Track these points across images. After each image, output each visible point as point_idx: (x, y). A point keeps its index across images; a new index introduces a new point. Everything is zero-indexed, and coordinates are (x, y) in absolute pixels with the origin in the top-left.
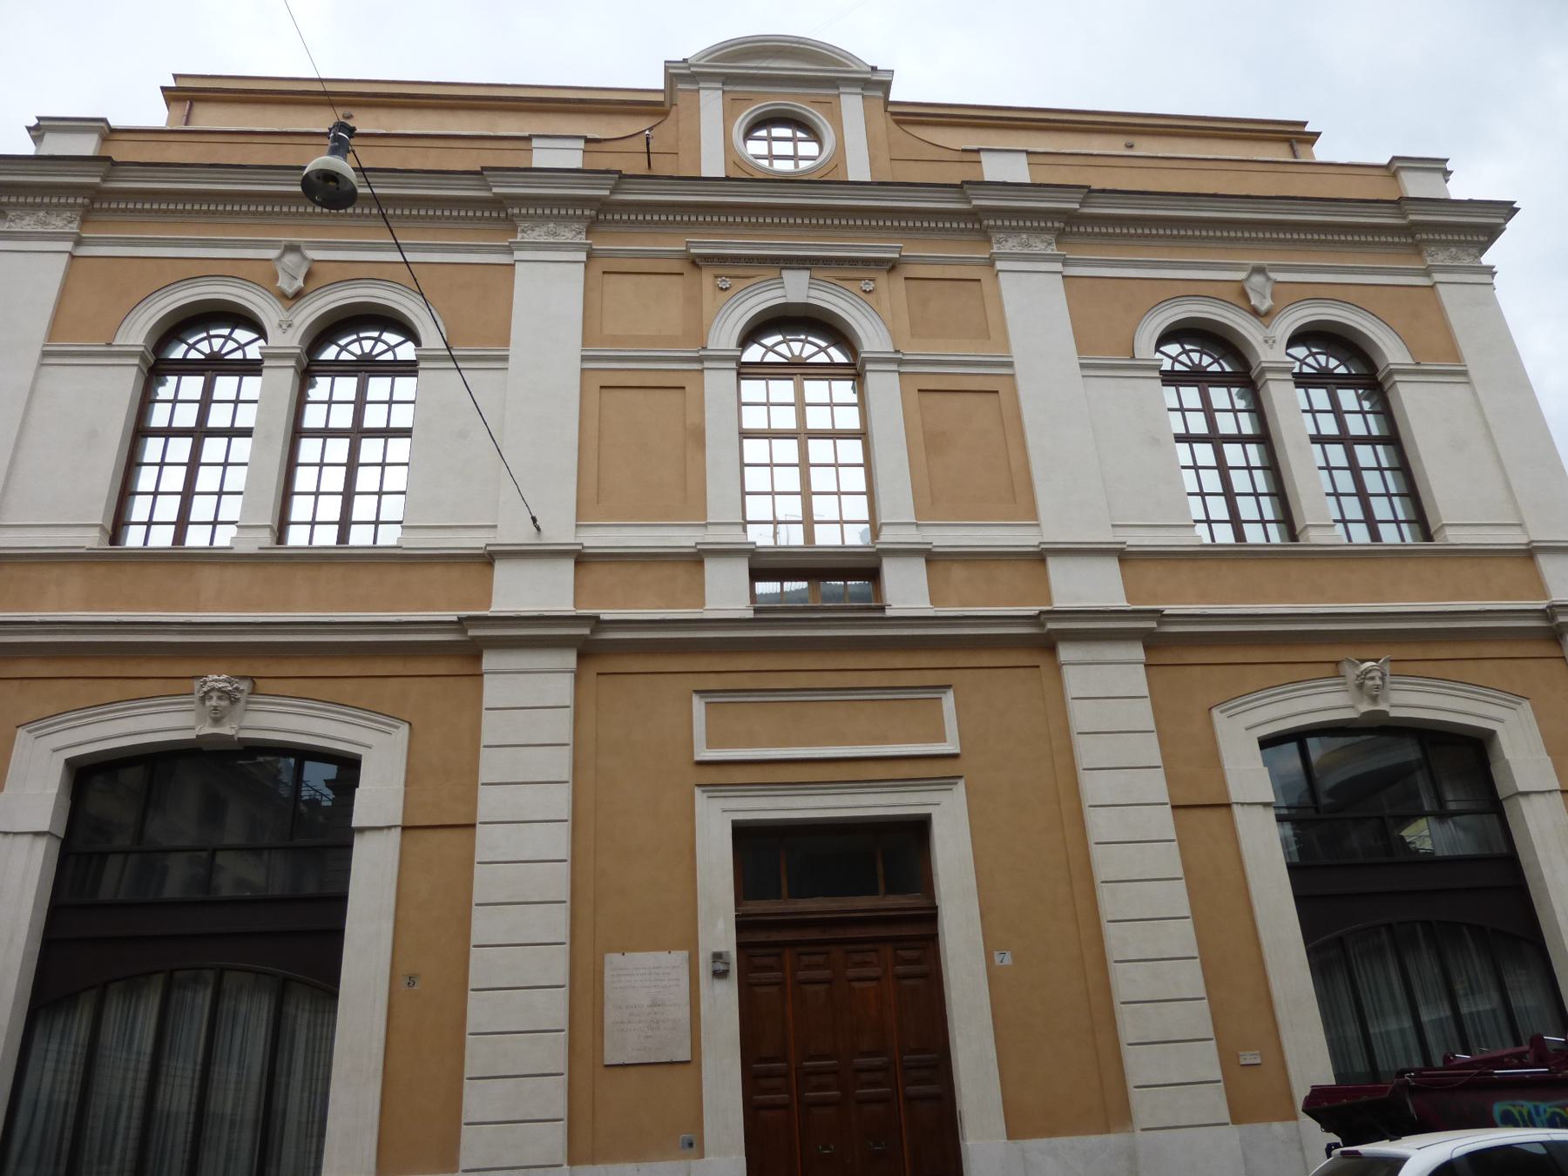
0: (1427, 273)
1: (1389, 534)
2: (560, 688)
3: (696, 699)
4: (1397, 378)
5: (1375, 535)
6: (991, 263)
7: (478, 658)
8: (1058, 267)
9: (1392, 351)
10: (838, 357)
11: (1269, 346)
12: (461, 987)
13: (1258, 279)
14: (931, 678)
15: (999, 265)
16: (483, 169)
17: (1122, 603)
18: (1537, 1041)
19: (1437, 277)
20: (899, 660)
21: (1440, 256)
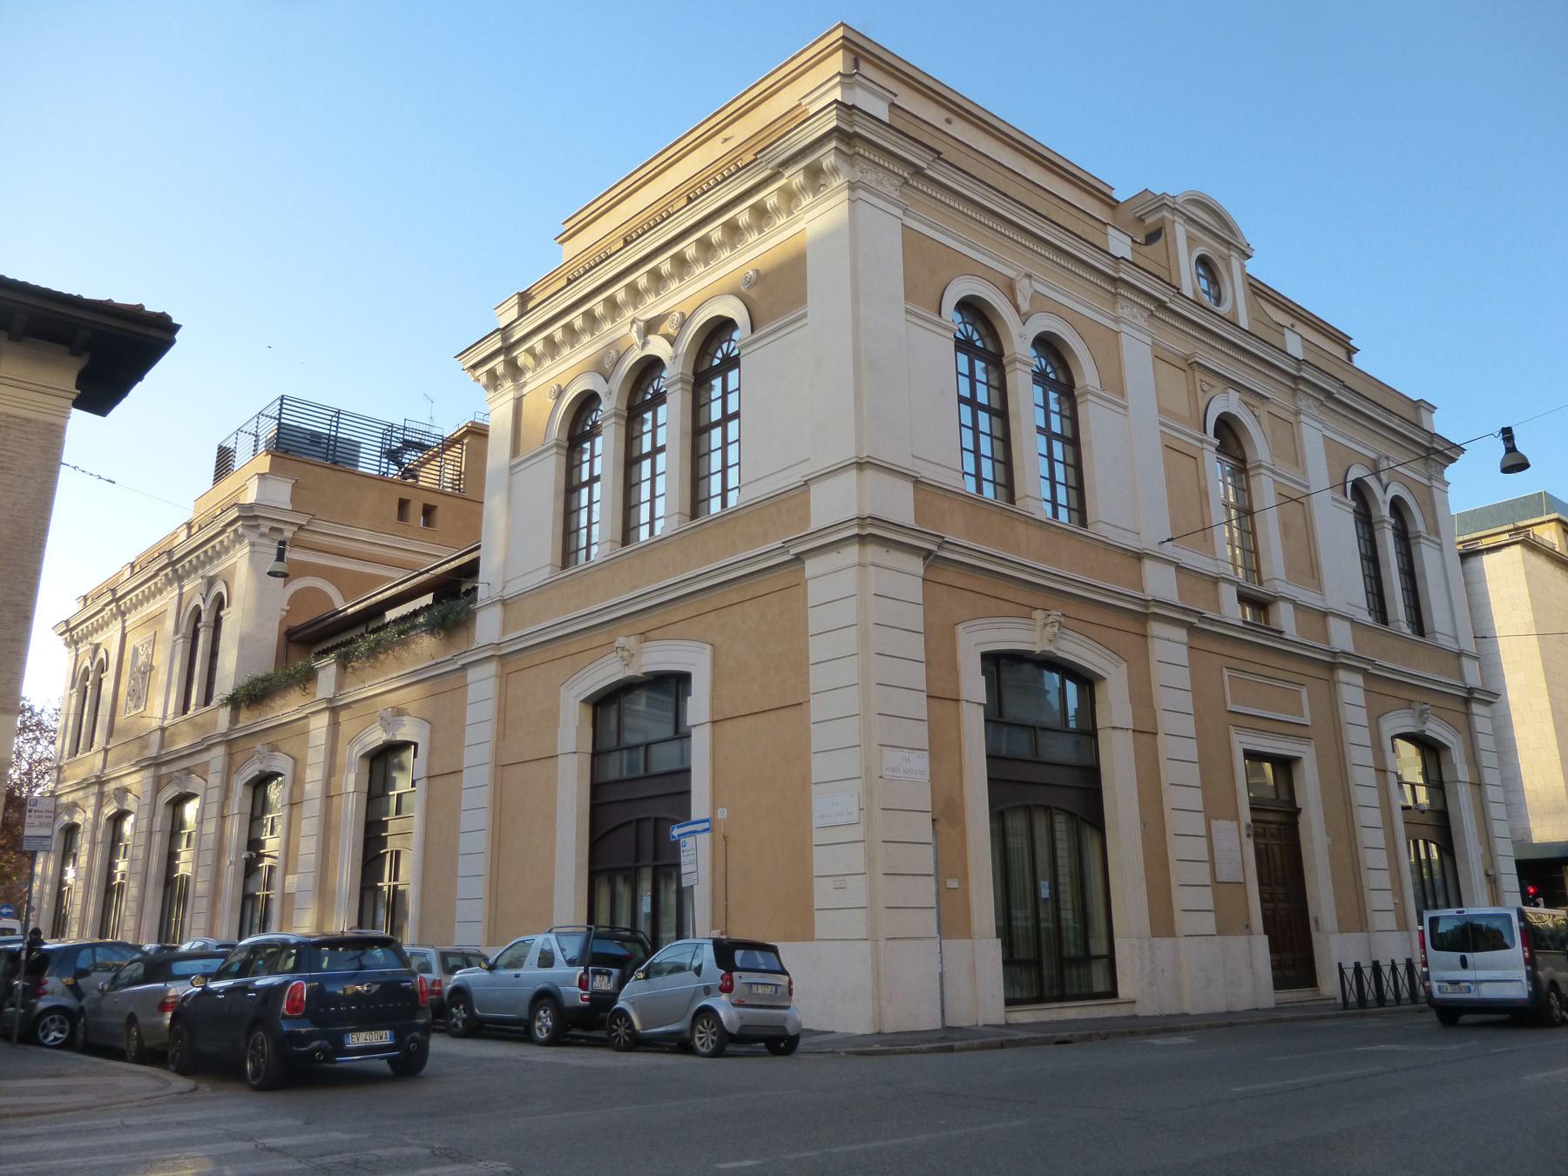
0: (1117, 320)
1: (988, 491)
2: (913, 588)
3: (1226, 672)
4: (1018, 365)
5: (979, 489)
6: (1297, 413)
7: (1144, 625)
8: (899, 212)
9: (1087, 375)
10: (1062, 379)
11: (1019, 343)
12: (805, 781)
13: (1026, 282)
14: (1298, 679)
15: (1303, 418)
16: (853, 107)
17: (909, 520)
18: (37, 786)
19: (1124, 327)
20: (1257, 657)
21: (1127, 311)
